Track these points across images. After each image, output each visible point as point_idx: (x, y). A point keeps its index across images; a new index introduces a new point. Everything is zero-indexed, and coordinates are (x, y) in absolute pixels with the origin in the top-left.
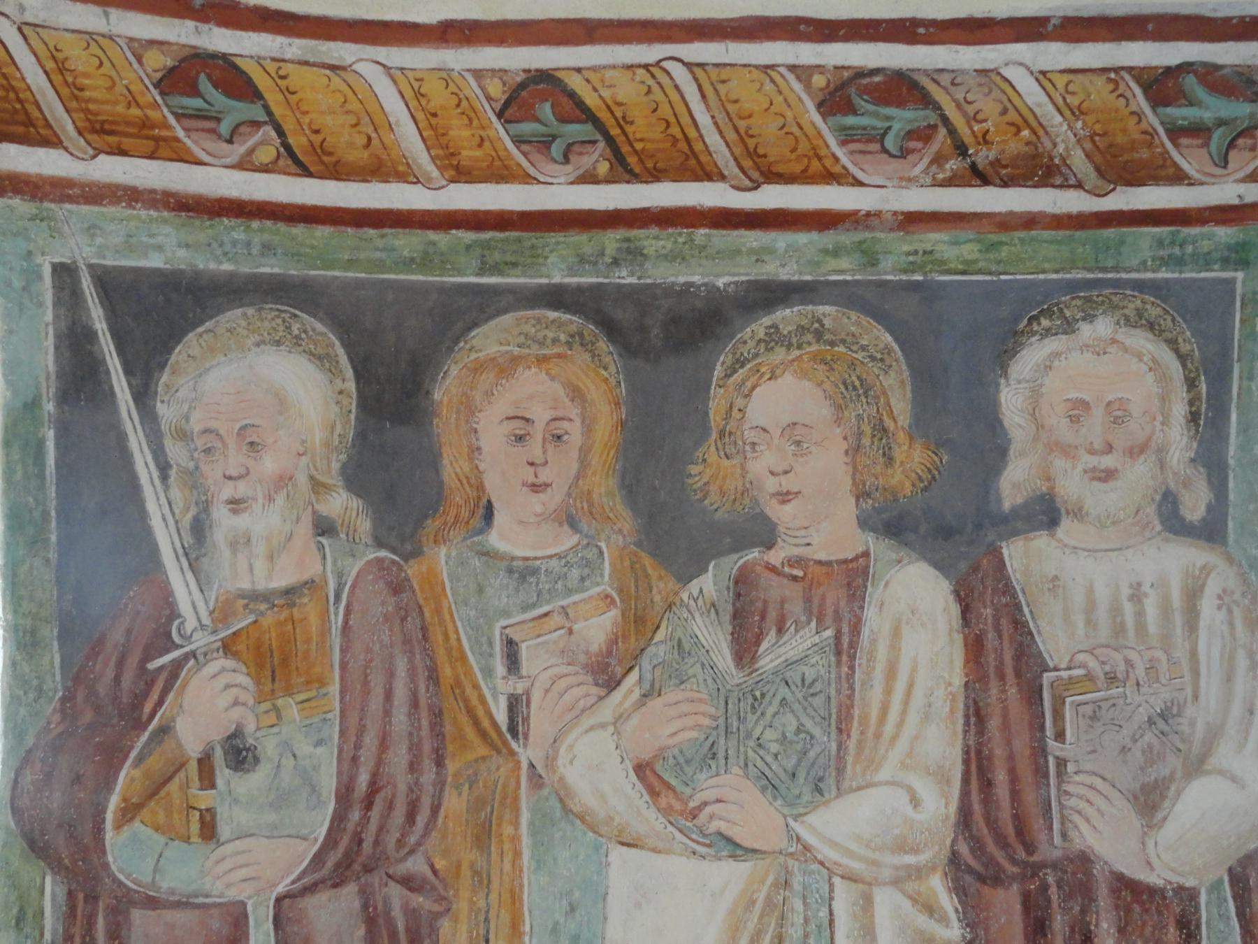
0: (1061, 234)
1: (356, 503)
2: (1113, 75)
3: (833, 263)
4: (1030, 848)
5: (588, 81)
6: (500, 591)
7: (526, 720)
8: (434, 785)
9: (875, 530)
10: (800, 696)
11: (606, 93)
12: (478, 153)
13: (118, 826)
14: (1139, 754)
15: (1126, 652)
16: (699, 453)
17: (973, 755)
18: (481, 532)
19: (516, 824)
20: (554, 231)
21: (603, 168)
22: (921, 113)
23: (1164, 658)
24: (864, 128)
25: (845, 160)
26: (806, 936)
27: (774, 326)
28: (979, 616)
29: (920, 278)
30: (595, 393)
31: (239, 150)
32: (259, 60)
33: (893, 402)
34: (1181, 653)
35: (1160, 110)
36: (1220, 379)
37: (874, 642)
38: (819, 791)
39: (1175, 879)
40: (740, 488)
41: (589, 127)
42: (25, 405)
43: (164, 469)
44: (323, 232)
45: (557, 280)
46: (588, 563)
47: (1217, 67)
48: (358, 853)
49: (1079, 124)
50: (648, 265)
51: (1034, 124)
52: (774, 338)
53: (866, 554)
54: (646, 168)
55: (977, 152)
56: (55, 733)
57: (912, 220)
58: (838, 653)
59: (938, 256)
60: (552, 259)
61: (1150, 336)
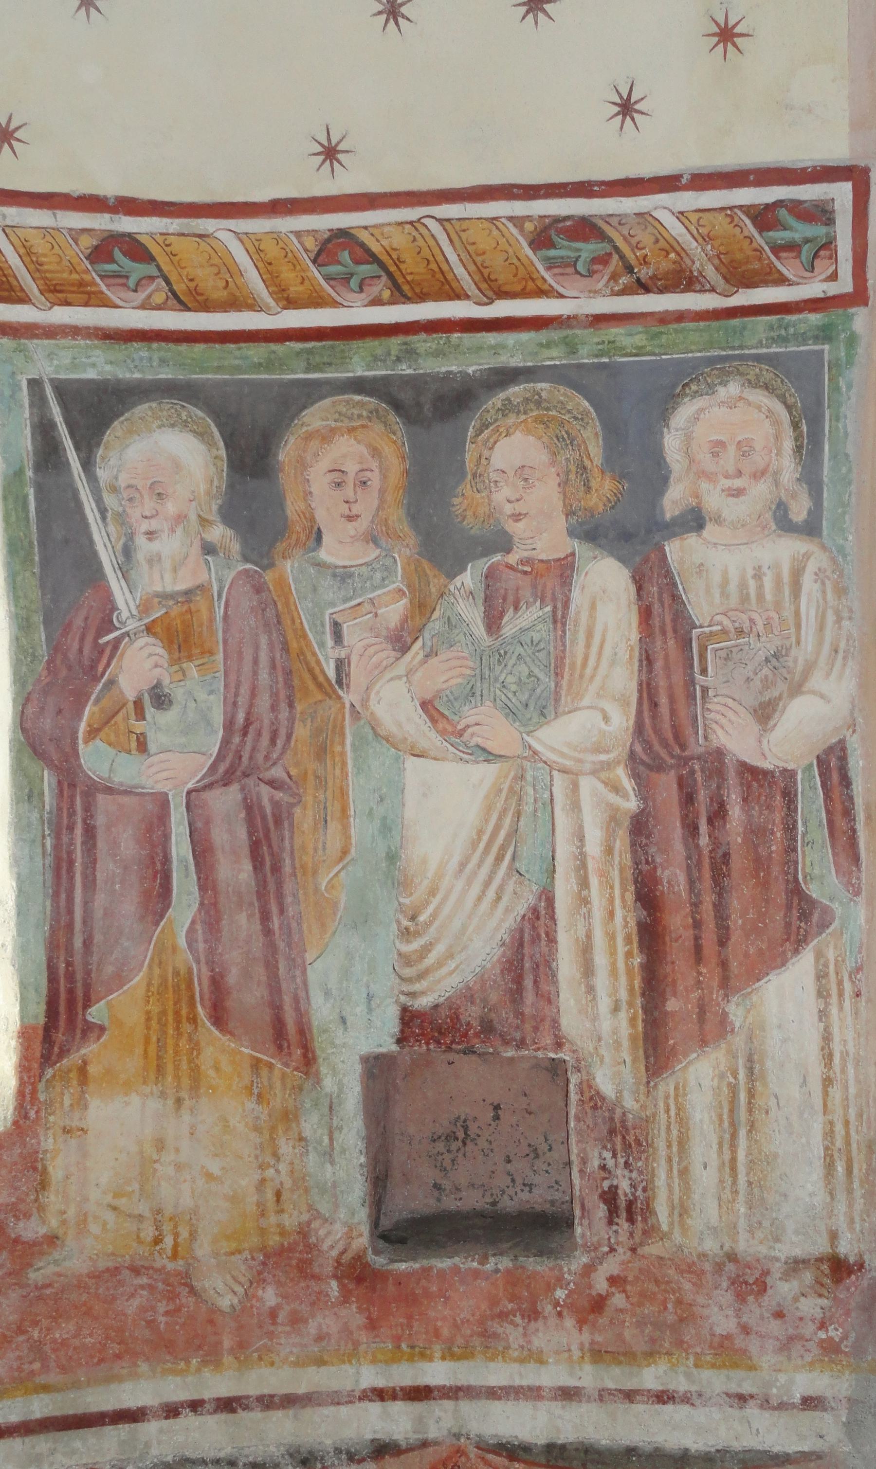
0: (702, 324)
1: (229, 532)
2: (729, 212)
3: (547, 353)
4: (683, 747)
5: (372, 235)
6: (328, 590)
7: (348, 675)
8: (288, 720)
9: (578, 537)
10: (530, 652)
11: (385, 243)
12: (301, 288)
13: (86, 742)
14: (758, 683)
15: (750, 613)
16: (459, 489)
17: (644, 686)
18: (314, 550)
19: (343, 743)
20: (355, 339)
21: (386, 294)
22: (600, 245)
23: (776, 617)
24: (562, 258)
25: (550, 280)
26: (536, 811)
27: (508, 399)
28: (649, 593)
29: (607, 360)
30: (388, 450)
31: (141, 296)
32: (151, 235)
33: (590, 448)
34: (788, 612)
35: (765, 234)
36: (815, 421)
37: (578, 613)
38: (543, 714)
39: (781, 764)
40: (487, 512)
41: (375, 266)
42: (15, 474)
43: (103, 512)
44: (199, 348)
45: (359, 373)
46: (387, 569)
47: (800, 202)
48: (239, 764)
49: (709, 247)
50: (420, 361)
51: (678, 249)
52: (507, 408)
53: (573, 554)
54: (416, 293)
55: (640, 271)
56: (44, 683)
57: (599, 320)
58: (555, 622)
59: (618, 344)
60: (356, 359)
61: (766, 393)
